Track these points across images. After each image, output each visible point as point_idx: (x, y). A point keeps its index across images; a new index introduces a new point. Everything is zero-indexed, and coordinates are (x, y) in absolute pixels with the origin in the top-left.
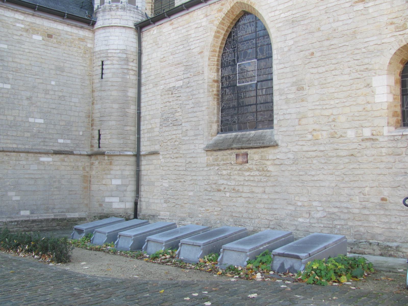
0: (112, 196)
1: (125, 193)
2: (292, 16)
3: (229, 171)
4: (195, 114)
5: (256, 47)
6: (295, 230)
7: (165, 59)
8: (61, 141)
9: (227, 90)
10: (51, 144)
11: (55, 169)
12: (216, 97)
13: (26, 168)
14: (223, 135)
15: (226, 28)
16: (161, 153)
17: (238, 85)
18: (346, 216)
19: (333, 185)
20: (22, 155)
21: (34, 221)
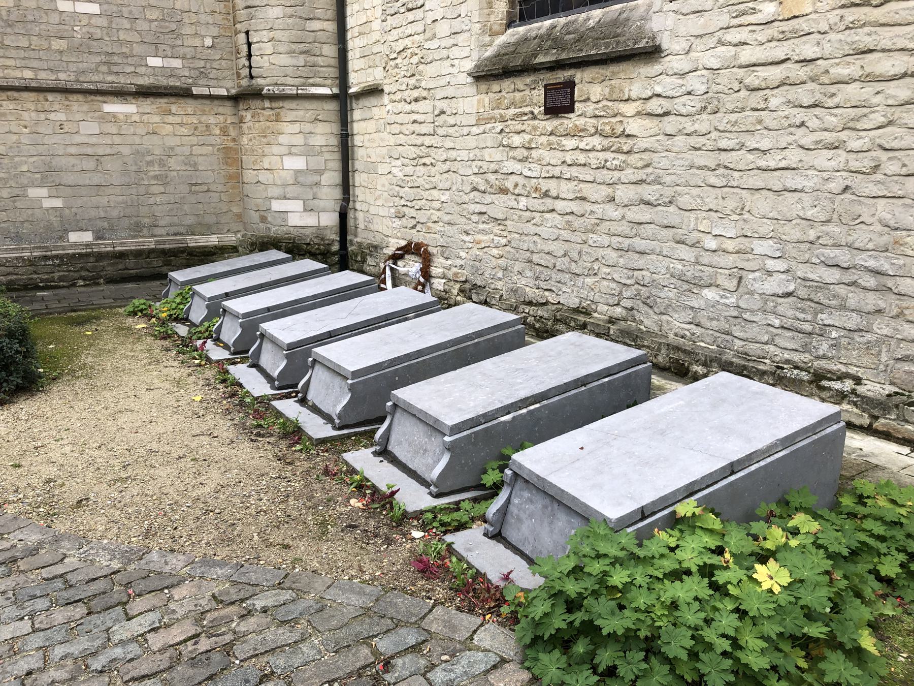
0: (285, 198)
3: (527, 137)
6: (690, 323)
10: (129, 69)
11: (148, 133)
13: (66, 129)
14: (521, 30)
16: (387, 89)
18: (872, 301)
19: (835, 186)
20: (50, 97)
21: (100, 256)
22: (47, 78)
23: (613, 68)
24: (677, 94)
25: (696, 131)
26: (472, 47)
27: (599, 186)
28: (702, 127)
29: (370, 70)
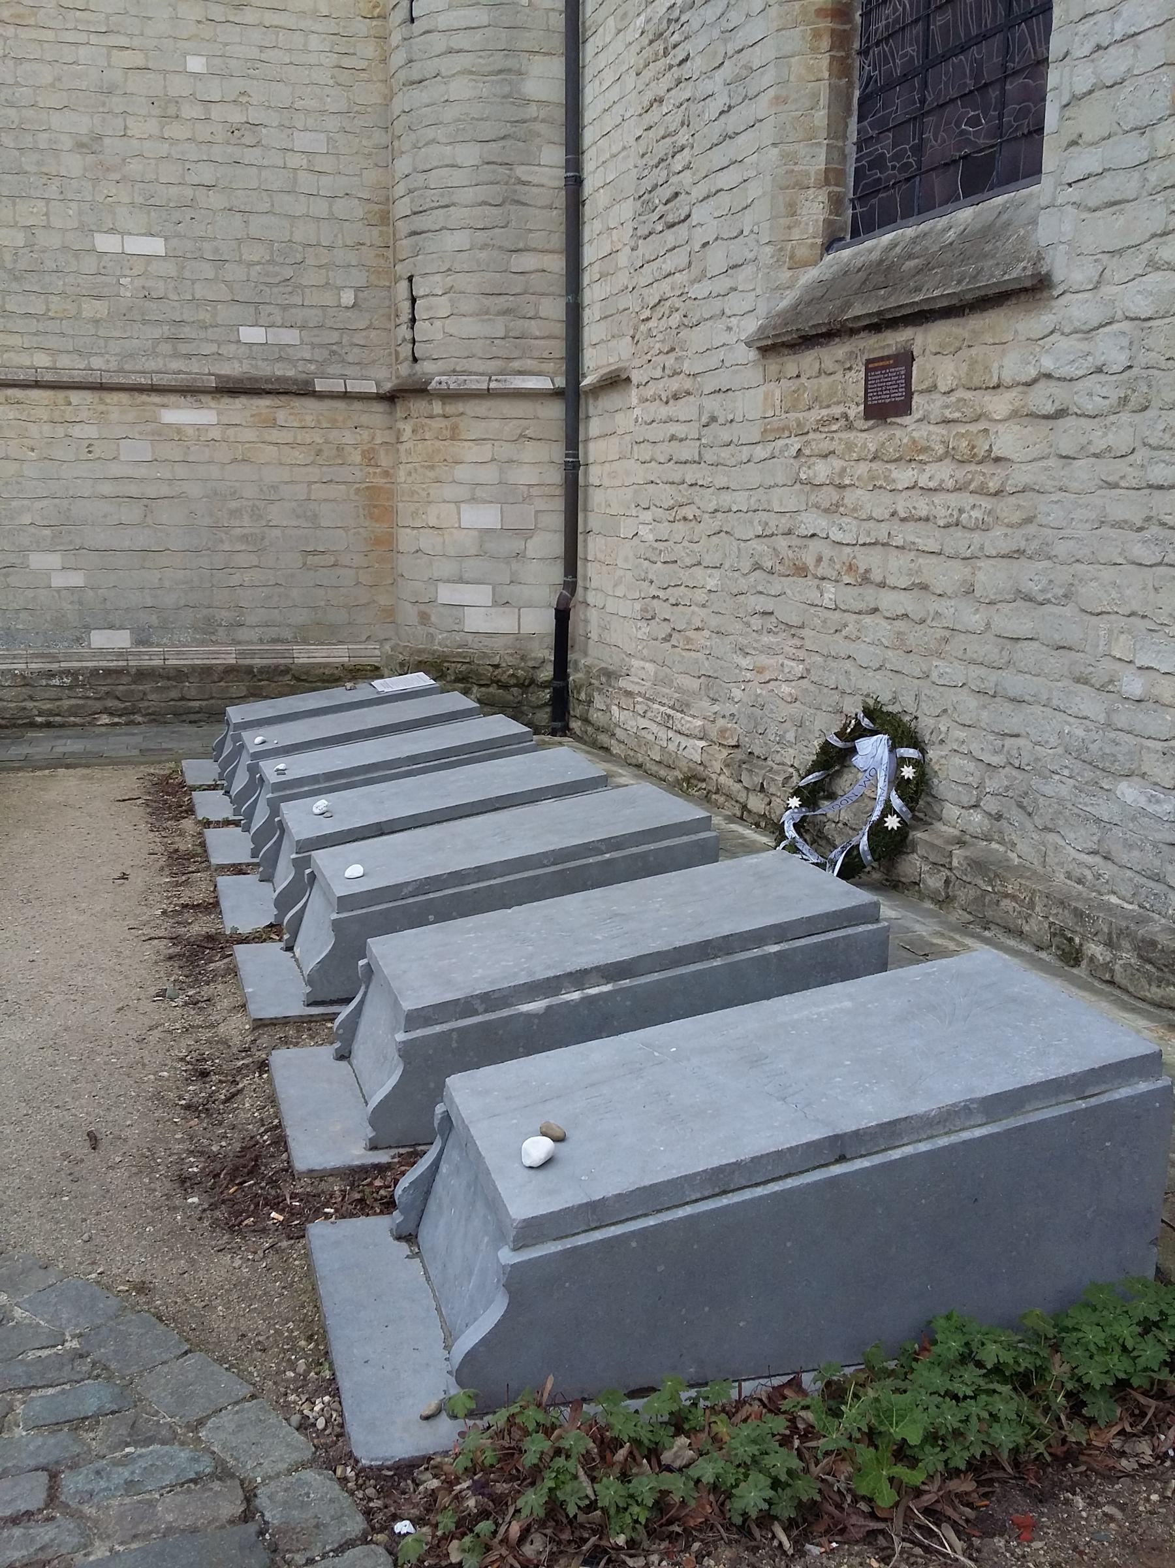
0: (461, 580)
1: (515, 566)
3: (837, 464)
6: (1094, 853)
8: (252, 335)
11: (234, 461)
12: (826, 24)
16: (636, 377)
20: (75, 397)
21: (142, 675)
22: (72, 366)
23: (975, 322)
24: (1080, 373)
25: (1109, 449)
26: (759, 291)
27: (950, 562)
28: (1120, 439)
29: (614, 342)
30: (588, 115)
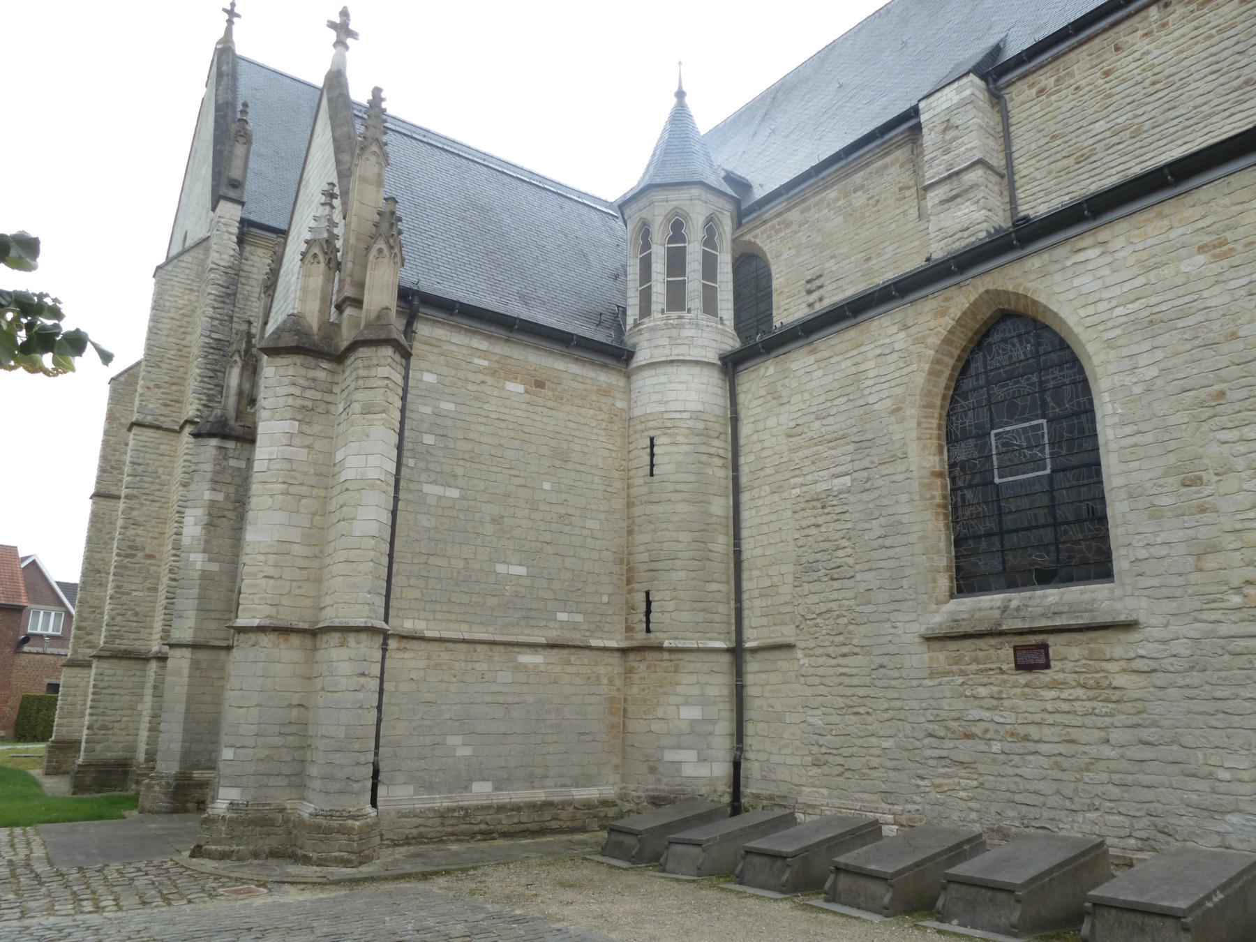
0: (680, 748)
2: (1149, 311)
3: (995, 689)
4: (890, 553)
5: (1043, 391)
7: (799, 429)
9: (969, 494)
15: (956, 353)
16: (801, 645)
17: (997, 481)
20: (479, 648)
21: (501, 808)
30: (744, 524)
